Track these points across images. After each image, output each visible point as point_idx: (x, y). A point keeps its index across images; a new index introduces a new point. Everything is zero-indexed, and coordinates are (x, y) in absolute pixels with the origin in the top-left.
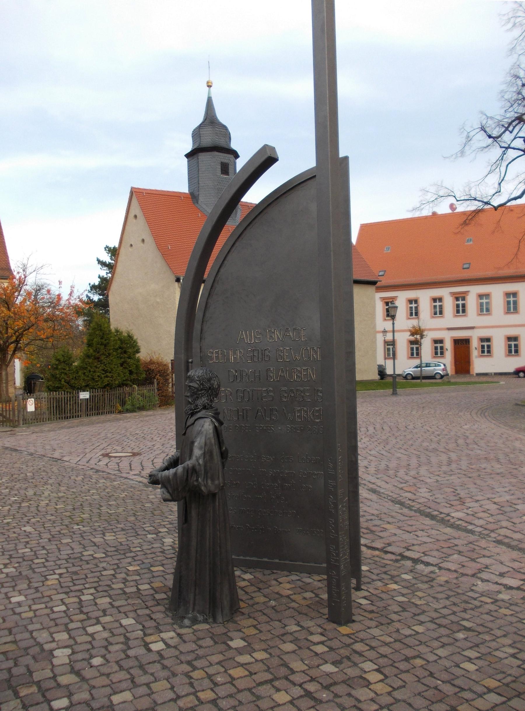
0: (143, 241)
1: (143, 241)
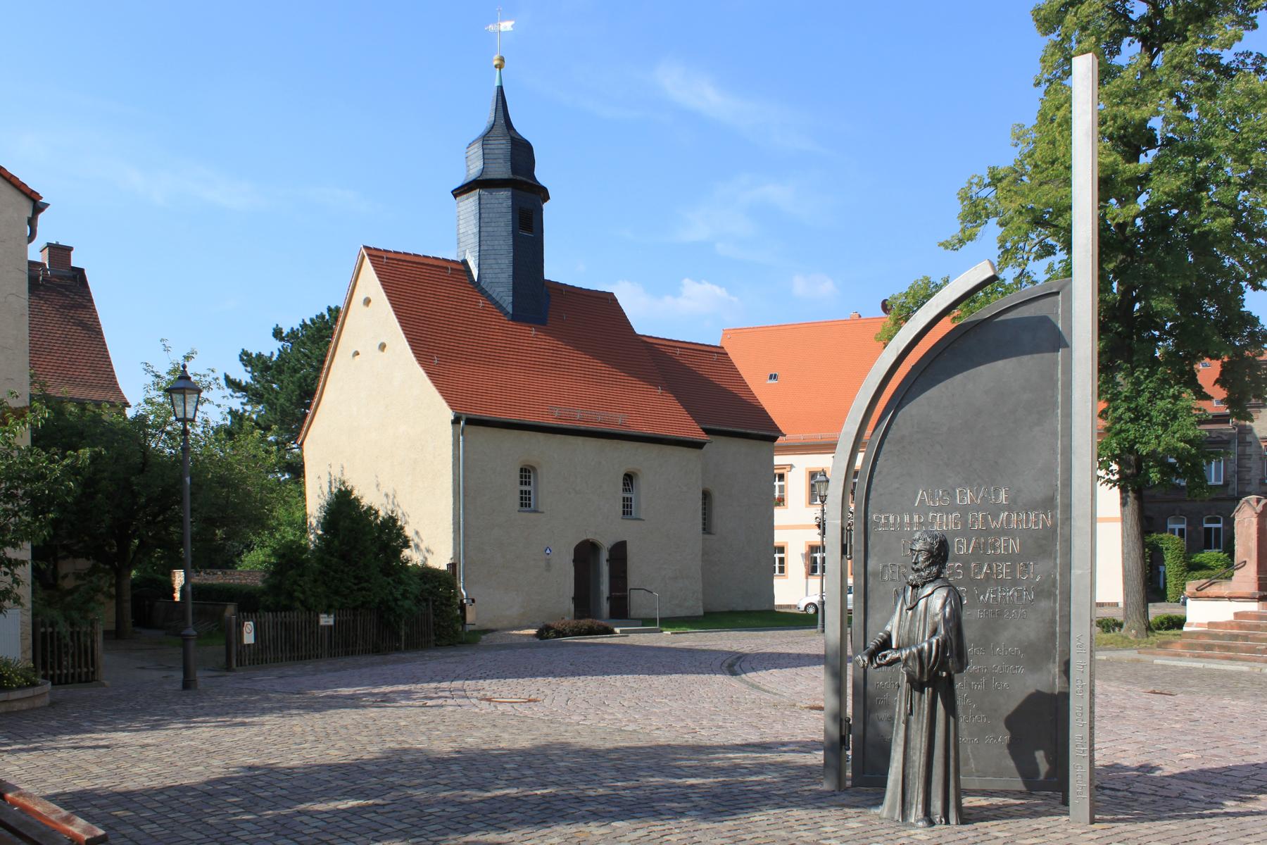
0: (382, 347)
1: (382, 347)
